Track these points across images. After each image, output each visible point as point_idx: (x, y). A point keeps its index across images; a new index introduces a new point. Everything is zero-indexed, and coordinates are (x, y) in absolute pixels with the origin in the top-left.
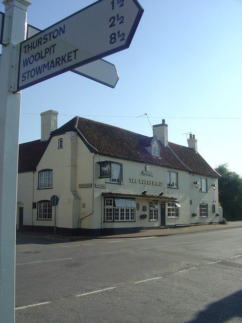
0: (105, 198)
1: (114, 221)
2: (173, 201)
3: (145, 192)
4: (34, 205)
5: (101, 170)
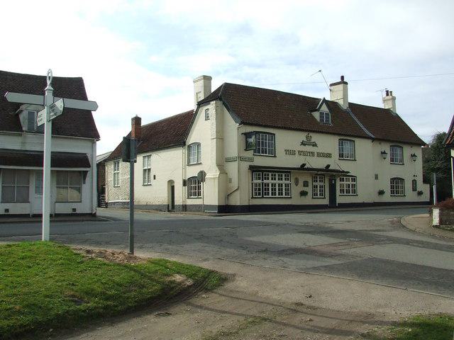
0: (253, 172)
1: (263, 197)
2: (343, 174)
3: (304, 165)
4: (185, 183)
5: (247, 142)
